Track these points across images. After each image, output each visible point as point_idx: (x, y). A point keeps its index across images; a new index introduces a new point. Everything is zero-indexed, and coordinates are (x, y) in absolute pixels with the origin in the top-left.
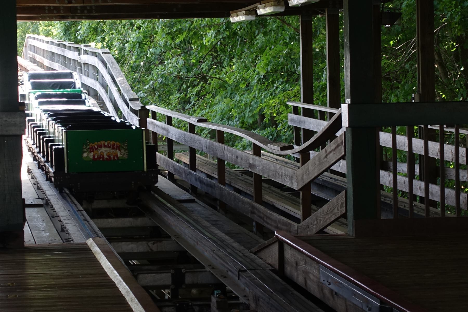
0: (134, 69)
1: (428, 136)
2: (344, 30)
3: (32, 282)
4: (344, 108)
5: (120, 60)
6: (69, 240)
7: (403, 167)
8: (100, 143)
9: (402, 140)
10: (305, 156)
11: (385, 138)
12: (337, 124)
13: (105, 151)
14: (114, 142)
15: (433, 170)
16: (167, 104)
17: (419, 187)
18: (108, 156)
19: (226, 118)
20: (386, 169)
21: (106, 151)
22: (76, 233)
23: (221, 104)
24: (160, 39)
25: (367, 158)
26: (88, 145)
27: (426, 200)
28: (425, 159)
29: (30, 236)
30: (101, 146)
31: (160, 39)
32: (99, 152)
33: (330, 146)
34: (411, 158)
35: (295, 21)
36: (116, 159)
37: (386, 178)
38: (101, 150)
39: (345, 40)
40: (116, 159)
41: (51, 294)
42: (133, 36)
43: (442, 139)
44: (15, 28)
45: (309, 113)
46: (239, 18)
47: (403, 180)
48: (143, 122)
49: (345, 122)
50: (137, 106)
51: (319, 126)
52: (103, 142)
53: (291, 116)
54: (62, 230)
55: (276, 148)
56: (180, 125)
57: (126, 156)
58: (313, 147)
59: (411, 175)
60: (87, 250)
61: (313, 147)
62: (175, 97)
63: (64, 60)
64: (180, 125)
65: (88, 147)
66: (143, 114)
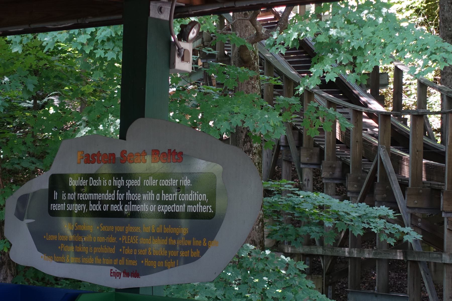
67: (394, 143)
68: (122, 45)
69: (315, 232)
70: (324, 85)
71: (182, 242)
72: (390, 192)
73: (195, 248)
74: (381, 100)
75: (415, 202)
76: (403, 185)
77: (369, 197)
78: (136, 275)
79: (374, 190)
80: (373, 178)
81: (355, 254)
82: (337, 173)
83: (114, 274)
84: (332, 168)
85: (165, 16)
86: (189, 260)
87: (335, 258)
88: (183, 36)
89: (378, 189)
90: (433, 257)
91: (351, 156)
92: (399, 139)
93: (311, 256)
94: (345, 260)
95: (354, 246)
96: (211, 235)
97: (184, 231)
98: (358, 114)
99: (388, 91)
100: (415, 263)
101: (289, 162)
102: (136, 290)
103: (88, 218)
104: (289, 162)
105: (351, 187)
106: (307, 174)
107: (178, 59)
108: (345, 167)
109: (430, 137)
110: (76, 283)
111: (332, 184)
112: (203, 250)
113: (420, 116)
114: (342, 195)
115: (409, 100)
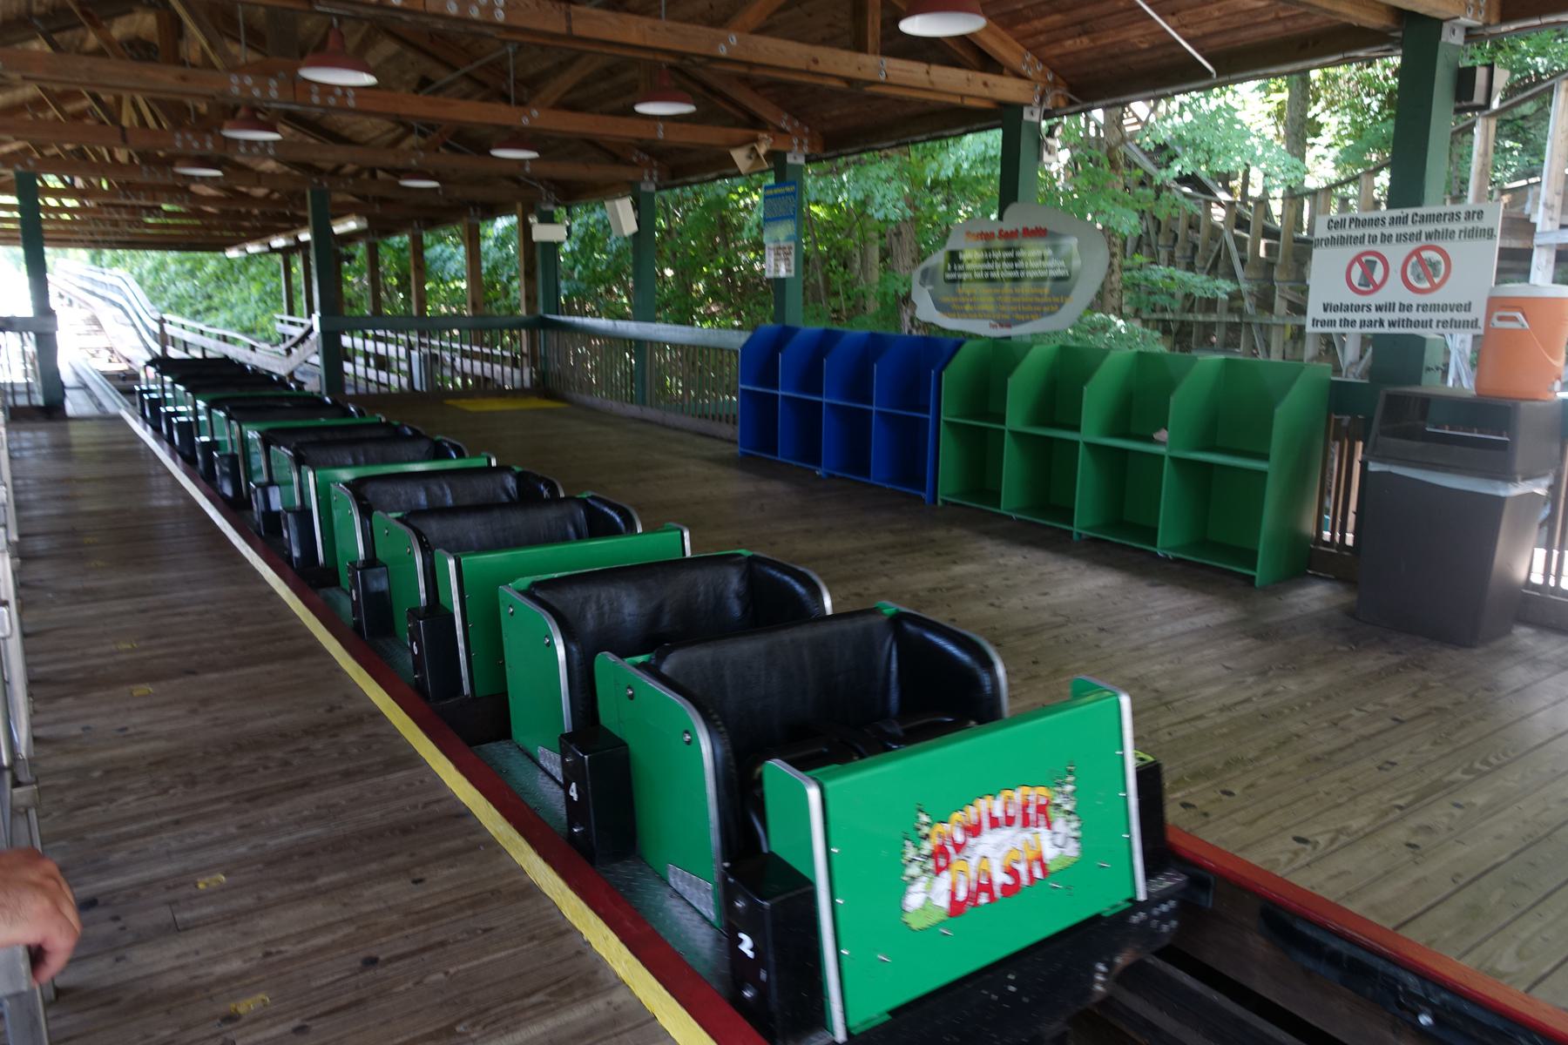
0: (153, 288)
1: (377, 339)
2: (313, 263)
3: (75, 441)
4: (316, 317)
5: (140, 281)
6: (106, 412)
7: (360, 360)
8: (971, 814)
9: (358, 342)
10: (289, 351)
11: (346, 341)
12: (311, 330)
13: (994, 852)
14: (1026, 790)
15: (383, 363)
16: (183, 315)
17: (372, 373)
18: (1013, 872)
19: (229, 325)
20: (348, 360)
21: (998, 847)
22: (111, 408)
23: (224, 315)
24: (172, 267)
25: (334, 355)
26: (926, 837)
27: (379, 383)
28: (377, 356)
29: (70, 409)
30: (974, 830)
31: (172, 267)
32: (974, 861)
33: (307, 343)
34: (366, 355)
35: (278, 258)
36: (1038, 873)
37: (348, 367)
38: (980, 850)
39: (314, 271)
40: (1038, 873)
41: (91, 449)
42: (149, 264)
43: (386, 340)
44: (42, 253)
45: (291, 323)
46: (233, 253)
47: (360, 370)
48: (162, 329)
49: (317, 329)
50: (157, 316)
51: (297, 332)
52: (983, 805)
53: (278, 325)
54: (100, 405)
55: (266, 346)
56: (193, 330)
57: (1072, 850)
58: (295, 345)
59: (367, 365)
60: (119, 418)
61: (295, 345)
62: (187, 310)
63: (92, 280)
64: (193, 330)
65: (927, 847)
66: (162, 322)
67: (1238, 226)
68: (345, 288)
69: (1162, 300)
70: (1183, 180)
71: (1046, 300)
72: (1232, 268)
73: (1053, 303)
74: (1230, 191)
75: (1252, 274)
76: (1243, 261)
77: (1213, 271)
78: (1009, 326)
79: (1218, 265)
80: (1218, 256)
81: (1200, 318)
82: (1189, 253)
83: (993, 326)
84: (1184, 249)
85: (1035, 119)
86: (1050, 313)
87: (1182, 323)
88: (1051, 134)
89: (1221, 265)
90: (1266, 318)
91: (1201, 238)
92: (1242, 223)
93: (1164, 321)
94: (1190, 324)
95: (1200, 311)
96: (1066, 294)
97: (1046, 291)
98: (1208, 203)
99: (1236, 184)
100: (1249, 324)
101: (1149, 245)
102: (1009, 338)
103: (1159, 589)
104: (1149, 245)
105: (1198, 263)
106: (1163, 254)
107: (1045, 154)
108: (1195, 248)
109: (1272, 221)
110: (963, 333)
111: (1183, 263)
112: (1060, 305)
113: (1262, 202)
114: (1190, 267)
115: (1255, 191)
